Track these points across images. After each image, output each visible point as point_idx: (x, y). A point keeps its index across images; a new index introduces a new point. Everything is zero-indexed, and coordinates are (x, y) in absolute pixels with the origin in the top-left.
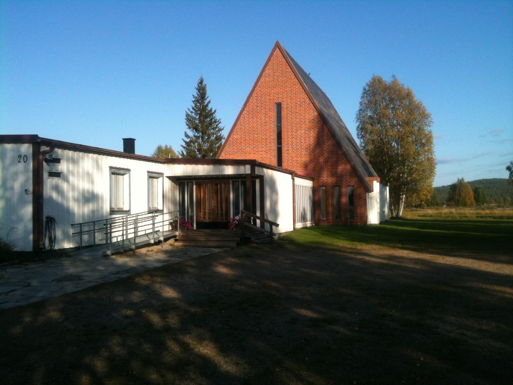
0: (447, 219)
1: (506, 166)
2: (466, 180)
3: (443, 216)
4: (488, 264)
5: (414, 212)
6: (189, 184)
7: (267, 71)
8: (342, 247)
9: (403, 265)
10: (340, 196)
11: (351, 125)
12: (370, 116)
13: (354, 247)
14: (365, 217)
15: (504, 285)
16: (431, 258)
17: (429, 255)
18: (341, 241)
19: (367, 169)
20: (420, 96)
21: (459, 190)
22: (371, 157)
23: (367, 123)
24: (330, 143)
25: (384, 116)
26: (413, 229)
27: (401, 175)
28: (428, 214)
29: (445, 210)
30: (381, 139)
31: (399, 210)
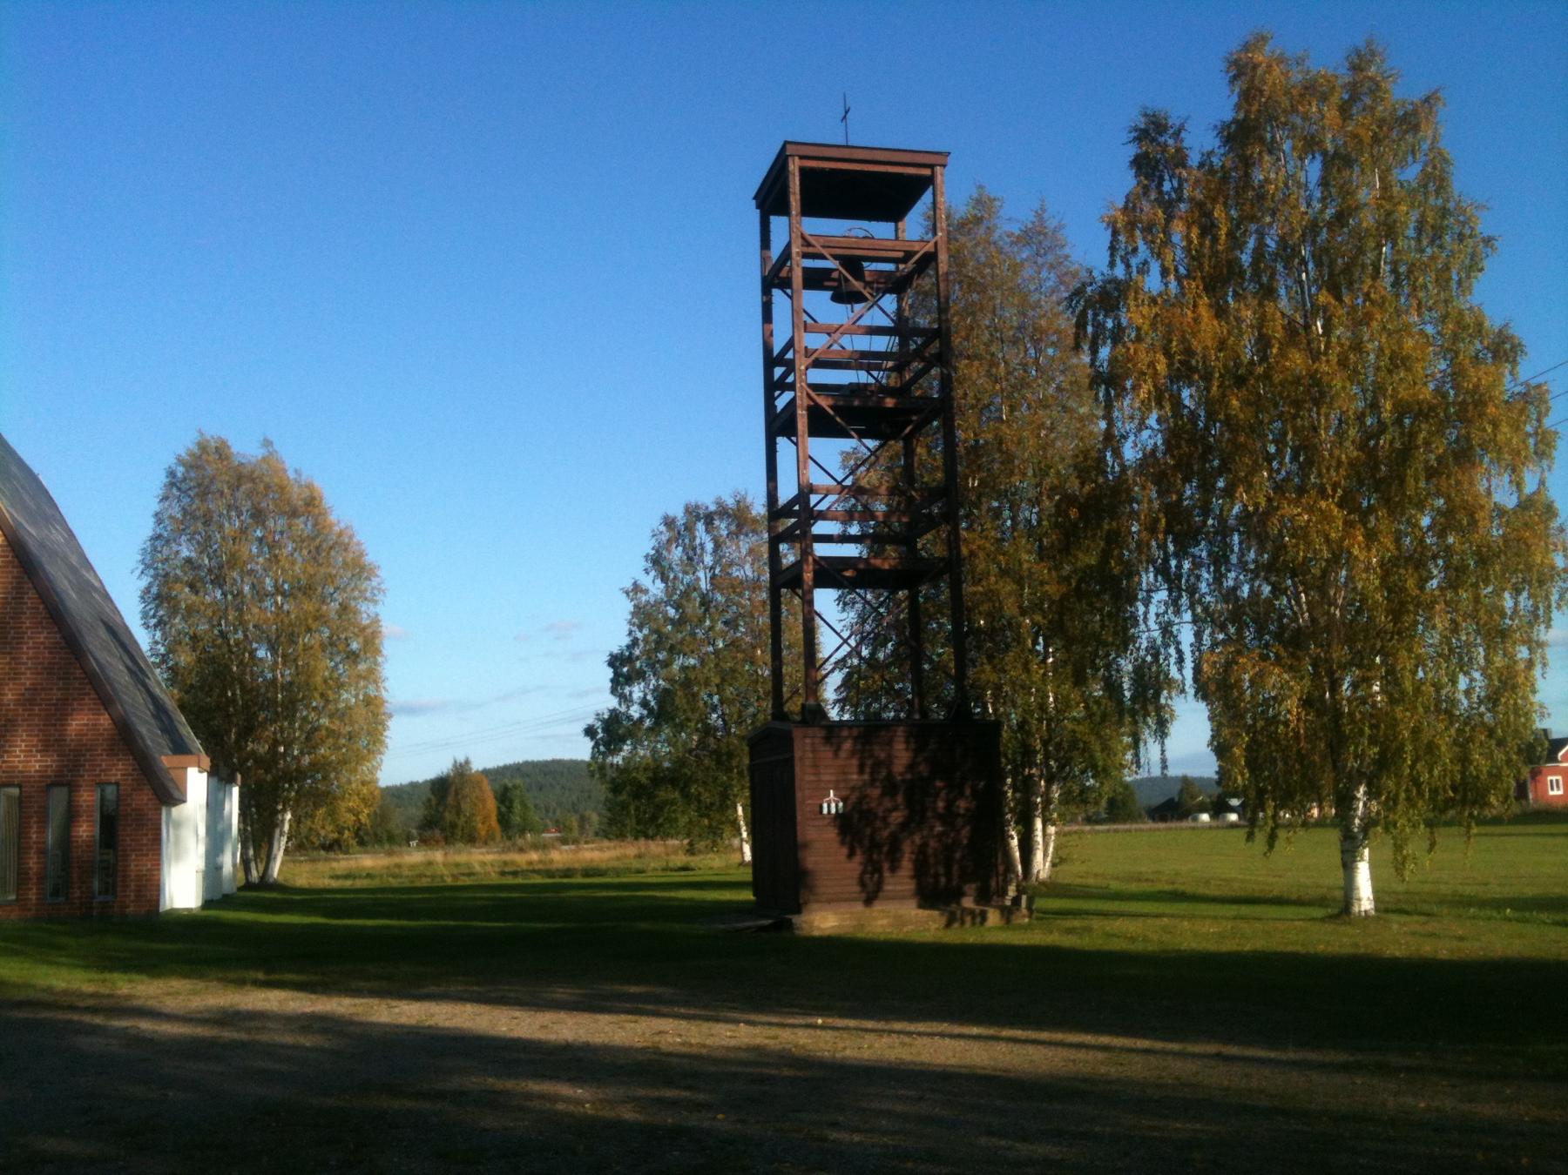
0: (418, 884)
1: (583, 725)
2: (477, 765)
3: (406, 873)
4: (518, 1014)
5: (321, 866)
8: (65, 992)
9: (264, 1038)
10: (71, 815)
11: (125, 589)
12: (188, 560)
13: (104, 990)
14: (151, 886)
15: (554, 1077)
16: (353, 1010)
17: (347, 1001)
18: (64, 972)
19: (169, 730)
20: (350, 508)
21: (457, 794)
22: (189, 689)
23: (177, 579)
25: (233, 561)
27: (282, 749)
28: (364, 868)
29: (414, 857)
30: (223, 635)
31: (269, 858)
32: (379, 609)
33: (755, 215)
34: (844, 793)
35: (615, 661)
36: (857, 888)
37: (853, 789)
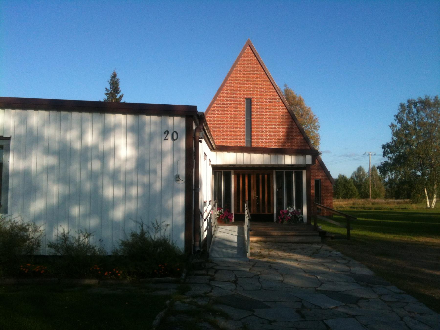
6: (217, 173)
7: (238, 67)
24: (298, 138)
26: (376, 220)
32: (318, 132)
35: (384, 147)
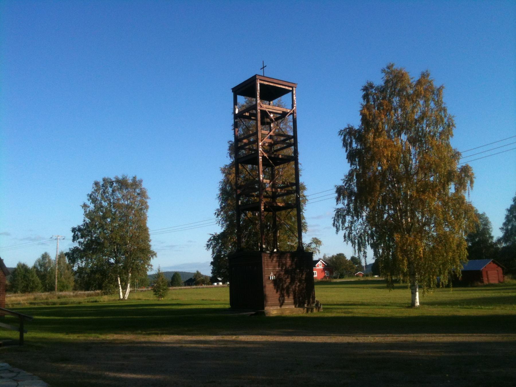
33: (232, 95)
34: (275, 273)
36: (278, 302)
37: (277, 272)
